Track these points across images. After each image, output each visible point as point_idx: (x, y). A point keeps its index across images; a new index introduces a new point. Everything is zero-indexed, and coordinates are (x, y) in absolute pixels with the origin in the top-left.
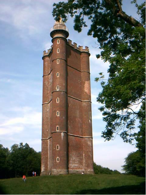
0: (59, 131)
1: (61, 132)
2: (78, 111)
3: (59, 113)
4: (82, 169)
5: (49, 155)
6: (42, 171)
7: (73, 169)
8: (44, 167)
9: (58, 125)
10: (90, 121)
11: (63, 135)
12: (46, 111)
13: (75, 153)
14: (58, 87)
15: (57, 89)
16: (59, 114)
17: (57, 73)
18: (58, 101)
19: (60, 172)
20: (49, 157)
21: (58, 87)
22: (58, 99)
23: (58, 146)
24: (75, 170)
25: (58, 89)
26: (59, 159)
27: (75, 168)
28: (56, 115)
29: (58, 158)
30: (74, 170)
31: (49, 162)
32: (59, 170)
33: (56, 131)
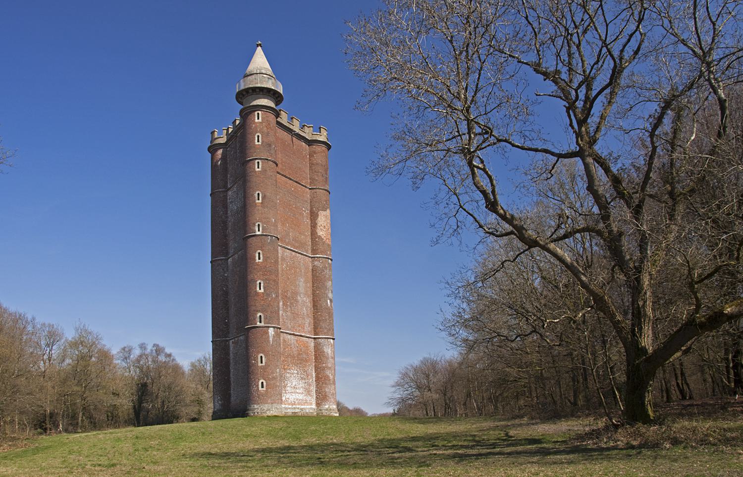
0: (262, 324)
1: (269, 327)
3: (262, 285)
4: (311, 404)
5: (231, 376)
11: (273, 333)
14: (259, 225)
16: (262, 288)
17: (257, 192)
18: (259, 259)
20: (232, 379)
21: (259, 225)
22: (259, 253)
23: (261, 357)
25: (259, 230)
26: (265, 384)
28: (256, 288)
29: (262, 383)
30: (294, 406)
33: (256, 324)
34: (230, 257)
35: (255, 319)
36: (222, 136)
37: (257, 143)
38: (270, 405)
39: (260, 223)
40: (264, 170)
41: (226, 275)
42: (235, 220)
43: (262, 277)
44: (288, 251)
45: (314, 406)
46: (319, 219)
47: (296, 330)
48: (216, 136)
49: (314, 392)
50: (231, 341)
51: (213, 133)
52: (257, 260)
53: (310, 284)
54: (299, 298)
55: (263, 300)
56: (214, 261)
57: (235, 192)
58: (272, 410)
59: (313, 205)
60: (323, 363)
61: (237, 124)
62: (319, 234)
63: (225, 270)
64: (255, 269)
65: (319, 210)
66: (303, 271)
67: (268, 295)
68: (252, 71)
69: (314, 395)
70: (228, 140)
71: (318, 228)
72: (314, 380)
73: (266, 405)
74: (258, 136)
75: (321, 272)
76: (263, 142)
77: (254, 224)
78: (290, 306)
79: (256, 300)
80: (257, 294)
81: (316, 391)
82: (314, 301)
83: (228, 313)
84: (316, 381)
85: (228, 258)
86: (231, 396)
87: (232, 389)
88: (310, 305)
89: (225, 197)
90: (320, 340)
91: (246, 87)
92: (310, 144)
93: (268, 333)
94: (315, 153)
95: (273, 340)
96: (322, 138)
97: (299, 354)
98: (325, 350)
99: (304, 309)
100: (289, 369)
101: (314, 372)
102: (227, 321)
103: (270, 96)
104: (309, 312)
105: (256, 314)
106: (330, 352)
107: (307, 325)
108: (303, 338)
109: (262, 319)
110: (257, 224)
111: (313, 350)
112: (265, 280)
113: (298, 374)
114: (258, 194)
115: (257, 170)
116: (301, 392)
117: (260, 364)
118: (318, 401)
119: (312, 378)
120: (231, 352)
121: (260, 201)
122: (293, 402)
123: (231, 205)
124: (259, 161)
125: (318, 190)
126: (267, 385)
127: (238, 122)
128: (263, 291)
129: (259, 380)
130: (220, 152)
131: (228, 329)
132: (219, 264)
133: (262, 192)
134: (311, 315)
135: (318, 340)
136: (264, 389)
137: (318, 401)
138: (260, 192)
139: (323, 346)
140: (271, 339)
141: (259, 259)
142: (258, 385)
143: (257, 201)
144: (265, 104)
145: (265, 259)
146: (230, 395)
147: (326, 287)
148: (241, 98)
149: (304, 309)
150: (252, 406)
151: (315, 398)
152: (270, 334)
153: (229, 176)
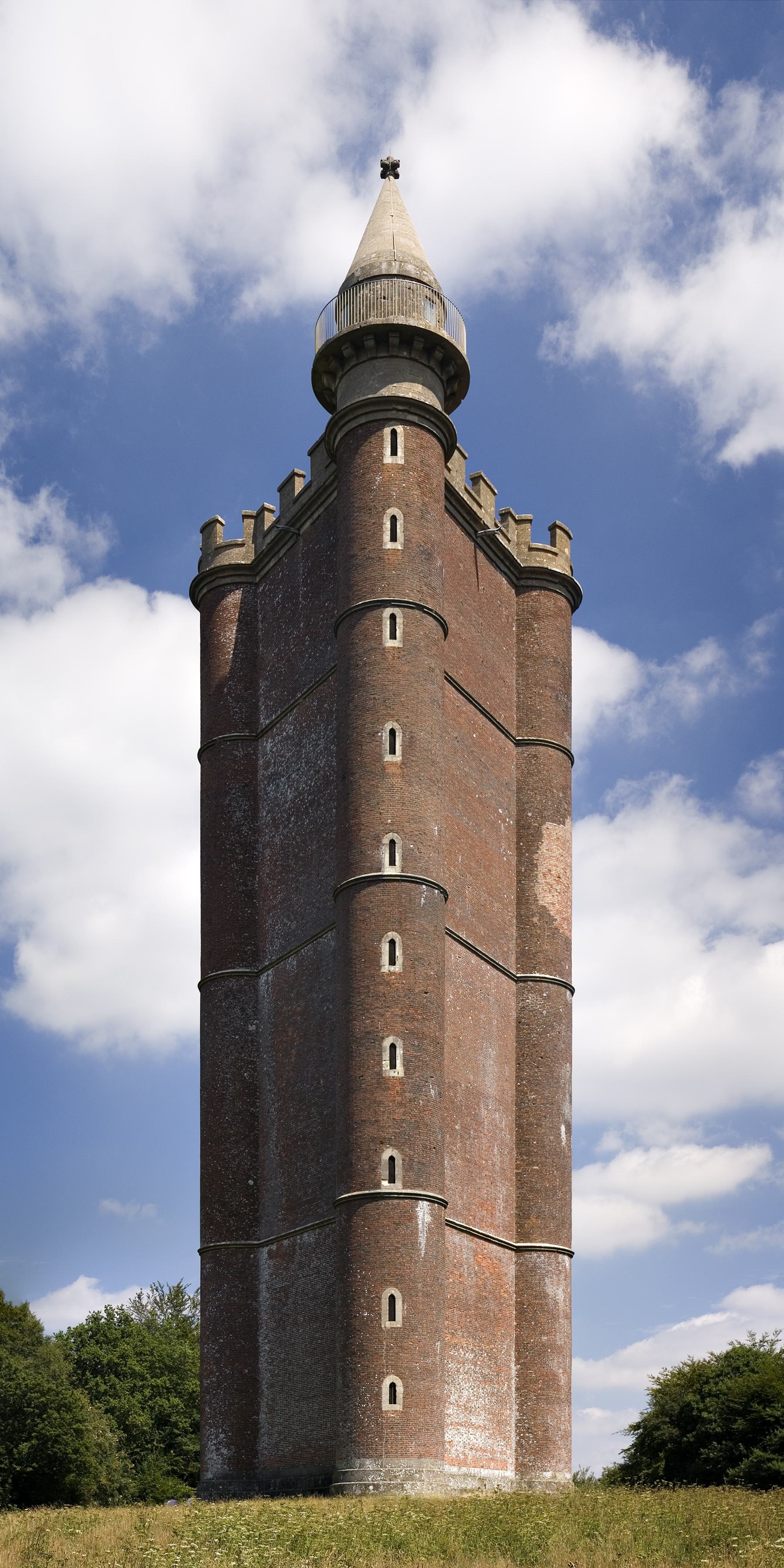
0: (397, 1188)
1: (417, 1198)
2: (493, 1053)
3: (399, 1052)
4: (504, 1467)
5: (263, 1364)
7: (461, 1463)
8: (228, 1446)
9: (396, 1146)
10: (563, 1128)
11: (428, 1219)
14: (392, 843)
16: (399, 1062)
17: (389, 726)
18: (392, 962)
20: (265, 1377)
21: (392, 843)
22: (392, 943)
23: (392, 1298)
25: (392, 862)
26: (400, 1390)
28: (380, 1063)
29: (393, 1386)
30: (464, 1470)
31: (271, 1410)
33: (378, 1186)
34: (266, 969)
35: (374, 1169)
36: (240, 540)
37: (389, 545)
38: (414, 1462)
39: (395, 836)
40: (410, 648)
41: (252, 1028)
42: (286, 837)
43: (399, 1027)
44: (460, 948)
45: (510, 1473)
46: (544, 848)
48: (220, 541)
49: (513, 1428)
50: (266, 1250)
51: (208, 528)
52: (386, 968)
53: (510, 1070)
54: (484, 1112)
55: (401, 1104)
56: (215, 979)
57: (288, 738)
59: (525, 799)
60: (542, 1333)
61: (297, 491)
62: (541, 903)
63: (249, 1011)
64: (377, 997)
65: (544, 819)
67: (418, 1089)
68: (372, 266)
69: (513, 1434)
70: (261, 558)
72: (513, 1389)
73: (403, 1461)
74: (394, 519)
75: (545, 1032)
76: (407, 541)
77: (378, 839)
78: (462, 1137)
79: (381, 1102)
80: (382, 1082)
81: (519, 1421)
82: (519, 1126)
83: (256, 1156)
84: (517, 1389)
85: (258, 975)
86: (258, 1430)
87: (264, 1408)
88: (508, 1137)
89: (251, 760)
90: (535, 1255)
91: (356, 325)
92: (522, 582)
93: (412, 1217)
94: (536, 616)
95: (427, 1245)
96: (559, 566)
97: (481, 1299)
98: (550, 1290)
99: (496, 1150)
101: (513, 1359)
102: (251, 1182)
103: (433, 370)
104: (507, 1159)
105: (378, 1153)
106: (561, 1296)
107: (501, 1204)
108: (491, 1245)
109: (399, 1171)
110: (386, 840)
111: (513, 1289)
112: (408, 1036)
113: (475, 1365)
114: (392, 732)
115: (390, 643)
116: (481, 1423)
117: (387, 1324)
119: (509, 1380)
120: (263, 1287)
121: (398, 757)
122: (462, 1457)
123: (271, 787)
124: (397, 611)
125: (541, 748)
126: (406, 1395)
127: (299, 485)
128: (402, 1074)
129: (383, 1375)
130: (235, 598)
131: (257, 1211)
132: (231, 990)
134: (511, 1173)
135: (527, 1255)
138: (396, 726)
139: (543, 1277)
140: (422, 1240)
141: (392, 962)
142: (379, 1395)
143: (388, 758)
144: (417, 397)
145: (412, 962)
146: (255, 1427)
147: (558, 1082)
148: (333, 375)
149: (496, 1150)
150: (358, 1462)
151: (514, 1445)
153: (263, 685)
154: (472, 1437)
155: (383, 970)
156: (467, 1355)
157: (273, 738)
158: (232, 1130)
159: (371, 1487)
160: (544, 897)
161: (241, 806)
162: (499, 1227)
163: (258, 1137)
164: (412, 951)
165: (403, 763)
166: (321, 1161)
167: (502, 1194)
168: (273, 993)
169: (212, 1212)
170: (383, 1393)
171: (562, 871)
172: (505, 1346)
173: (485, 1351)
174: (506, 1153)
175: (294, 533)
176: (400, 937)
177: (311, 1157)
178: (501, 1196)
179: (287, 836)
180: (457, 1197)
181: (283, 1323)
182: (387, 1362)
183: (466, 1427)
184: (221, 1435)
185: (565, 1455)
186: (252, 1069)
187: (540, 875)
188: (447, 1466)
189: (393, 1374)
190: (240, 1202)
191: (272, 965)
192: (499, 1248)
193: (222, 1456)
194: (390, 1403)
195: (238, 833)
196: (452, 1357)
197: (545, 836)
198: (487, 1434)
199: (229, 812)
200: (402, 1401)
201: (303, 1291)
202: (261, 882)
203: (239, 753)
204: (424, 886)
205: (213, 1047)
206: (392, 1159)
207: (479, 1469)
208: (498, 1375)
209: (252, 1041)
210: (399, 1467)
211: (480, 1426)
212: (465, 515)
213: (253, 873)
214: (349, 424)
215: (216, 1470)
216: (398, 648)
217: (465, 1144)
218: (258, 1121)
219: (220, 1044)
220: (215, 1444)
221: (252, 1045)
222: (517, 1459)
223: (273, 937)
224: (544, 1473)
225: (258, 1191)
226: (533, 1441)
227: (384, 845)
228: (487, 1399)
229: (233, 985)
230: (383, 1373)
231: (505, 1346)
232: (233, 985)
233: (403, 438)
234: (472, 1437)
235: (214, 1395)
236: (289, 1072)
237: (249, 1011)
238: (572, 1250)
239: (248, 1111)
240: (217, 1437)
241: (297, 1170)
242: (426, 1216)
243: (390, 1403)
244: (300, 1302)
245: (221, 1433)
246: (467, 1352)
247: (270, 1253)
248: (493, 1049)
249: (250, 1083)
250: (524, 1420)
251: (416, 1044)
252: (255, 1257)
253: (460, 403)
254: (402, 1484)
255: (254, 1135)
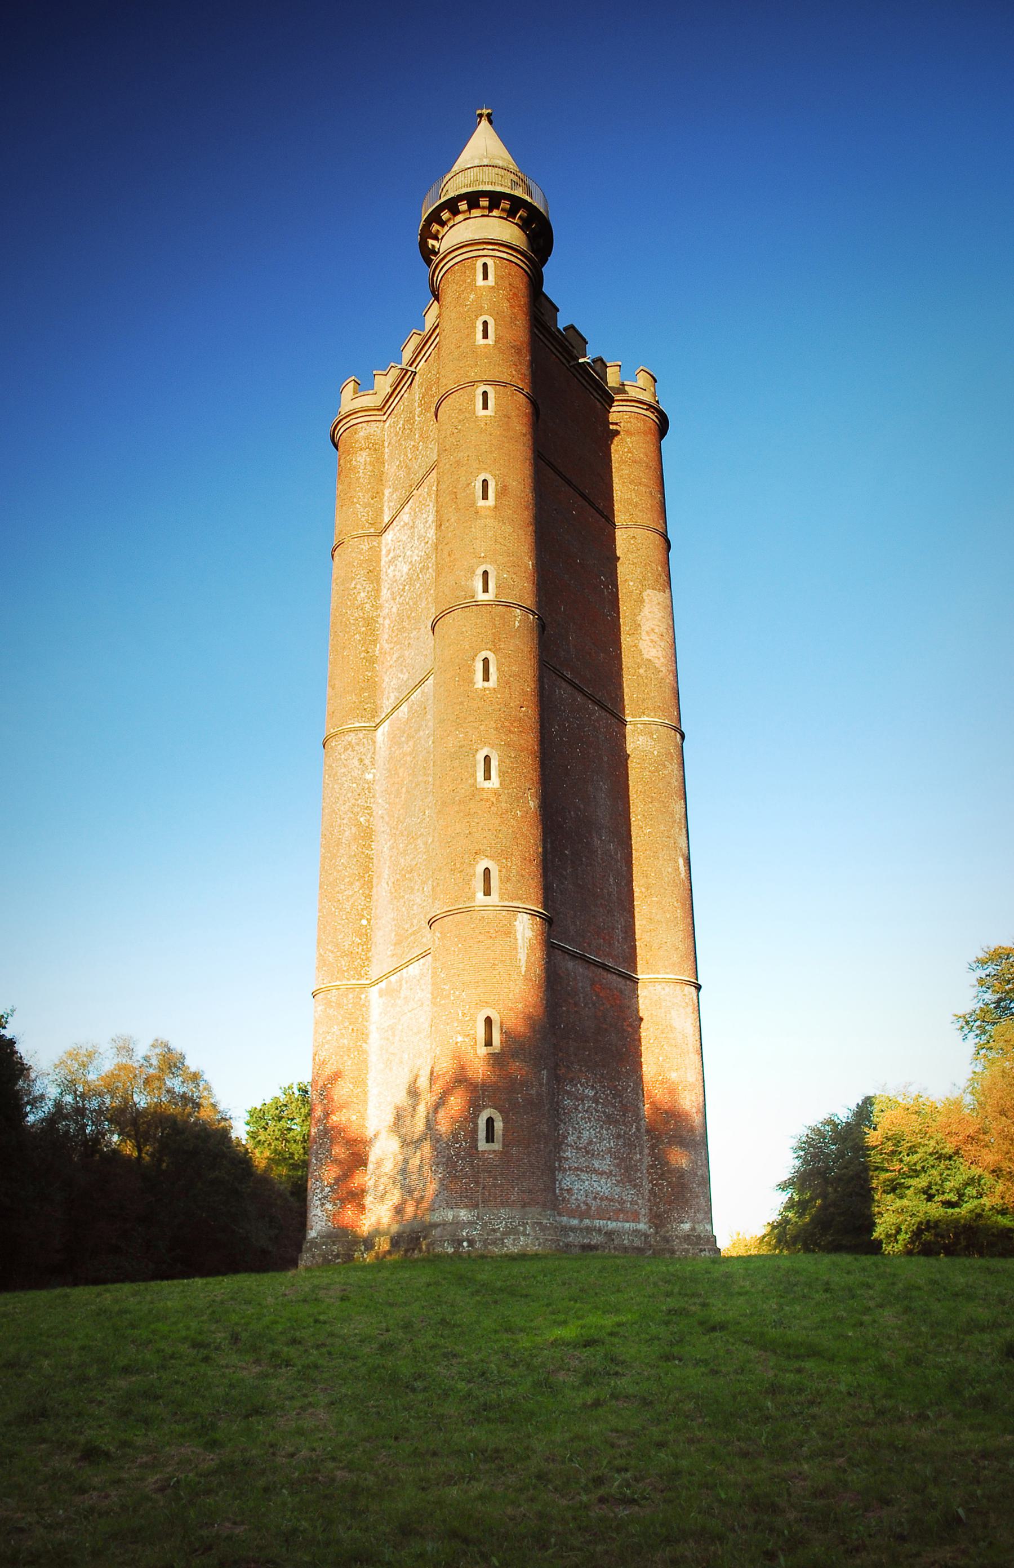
3: (494, 764)
4: (636, 1219)
6: (312, 1234)
12: (354, 780)
13: (592, 1093)
15: (481, 406)
17: (481, 477)
19: (512, 1231)
24: (598, 1223)
26: (499, 1125)
27: (594, 1204)
28: (474, 775)
29: (490, 1122)
30: (587, 1222)
32: (502, 1218)
33: (472, 897)
34: (382, 721)
41: (369, 777)
47: (589, 945)
54: (597, 842)
58: (525, 1235)
62: (646, 656)
66: (606, 759)
71: (644, 636)
83: (370, 896)
85: (377, 727)
89: (375, 551)
100: (572, 1080)
102: (364, 922)
113: (597, 1102)
116: (606, 1168)
118: (657, 1204)
122: (584, 1207)
131: (369, 950)
132: (350, 743)
133: (494, 476)
136: (497, 1146)
137: (657, 1204)
152: (519, 937)
153: (387, 492)
154: (595, 1185)
155: (476, 686)
156: (587, 1091)
157: (393, 530)
158: (347, 872)
159: (465, 1244)
160: (649, 651)
161: (365, 588)
162: (618, 957)
163: (372, 878)
164: (506, 668)
165: (496, 507)
166: (425, 889)
167: (621, 924)
168: (388, 741)
169: (325, 953)
170: (479, 1130)
171: (665, 631)
172: (632, 1084)
173: (608, 1088)
174: (623, 884)
175: (412, 372)
176: (494, 656)
177: (416, 887)
178: (620, 926)
179: (403, 603)
180: (569, 922)
181: (390, 1063)
182: (483, 1094)
183: (588, 1172)
184: (326, 1189)
185: (704, 1204)
186: (368, 814)
187: (644, 633)
188: (565, 1218)
189: (491, 1107)
190: (353, 942)
191: (387, 716)
192: (620, 979)
193: (326, 1213)
194: (487, 1142)
195: (361, 610)
196: (568, 1092)
197: (647, 601)
198: (614, 1182)
199: (354, 593)
200: (501, 1139)
201: (408, 1026)
202: (381, 648)
203: (365, 547)
204: (518, 611)
205: (332, 796)
206: (487, 871)
207: (605, 1222)
208: (624, 1115)
209: (369, 788)
210: (499, 1219)
211: (605, 1172)
212: (557, 347)
213: (375, 642)
214: (447, 265)
215: (320, 1228)
216: (491, 416)
217: (577, 869)
218: (372, 863)
219: (338, 793)
220: (320, 1199)
221: (369, 792)
222: (651, 1210)
223: (389, 693)
224: (682, 1225)
225: (372, 931)
226: (667, 1189)
227: (476, 575)
228: (612, 1141)
229: (352, 739)
230: (479, 1106)
231: (632, 1084)
232: (352, 739)
233: (493, 269)
234: (595, 1185)
235: (321, 1144)
236: (399, 810)
237: (367, 762)
238: (699, 983)
239: (363, 853)
240: (322, 1190)
241: (405, 903)
242: (526, 931)
243: (487, 1142)
244: (405, 1039)
245: (327, 1186)
246: (587, 1088)
247: (380, 991)
248: (604, 784)
249: (367, 827)
250: (656, 1165)
251: (513, 756)
252: (366, 997)
253: (547, 259)
254: (503, 1240)
255: (369, 876)
